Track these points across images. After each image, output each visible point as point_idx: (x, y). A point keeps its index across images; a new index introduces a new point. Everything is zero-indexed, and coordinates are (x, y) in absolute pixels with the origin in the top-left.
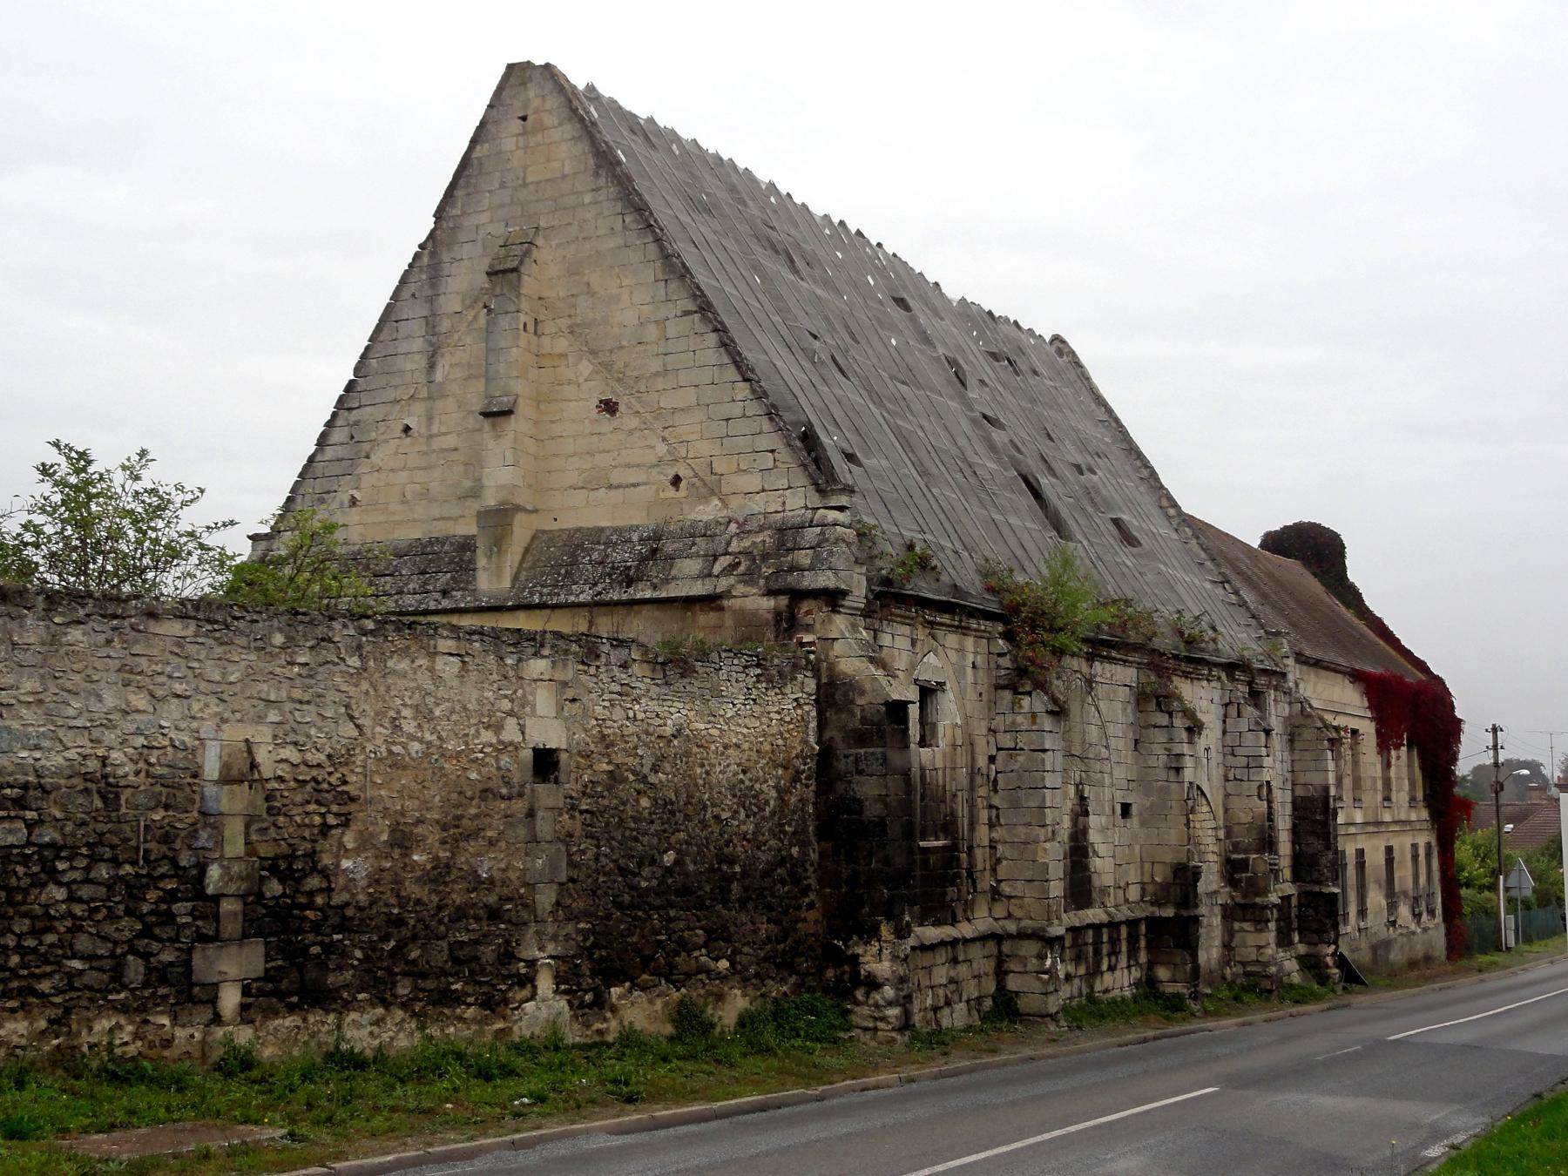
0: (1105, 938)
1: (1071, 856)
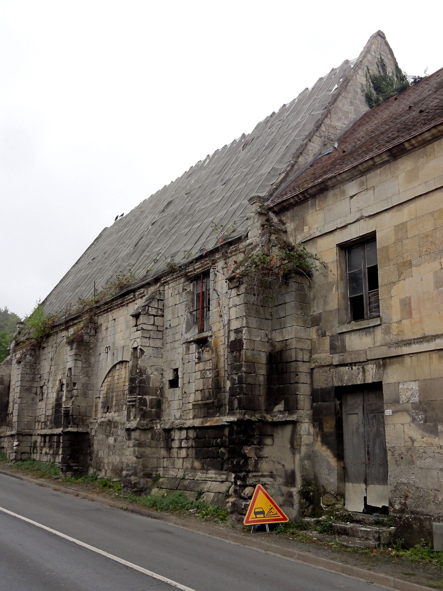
0: (47, 440)
1: (55, 407)
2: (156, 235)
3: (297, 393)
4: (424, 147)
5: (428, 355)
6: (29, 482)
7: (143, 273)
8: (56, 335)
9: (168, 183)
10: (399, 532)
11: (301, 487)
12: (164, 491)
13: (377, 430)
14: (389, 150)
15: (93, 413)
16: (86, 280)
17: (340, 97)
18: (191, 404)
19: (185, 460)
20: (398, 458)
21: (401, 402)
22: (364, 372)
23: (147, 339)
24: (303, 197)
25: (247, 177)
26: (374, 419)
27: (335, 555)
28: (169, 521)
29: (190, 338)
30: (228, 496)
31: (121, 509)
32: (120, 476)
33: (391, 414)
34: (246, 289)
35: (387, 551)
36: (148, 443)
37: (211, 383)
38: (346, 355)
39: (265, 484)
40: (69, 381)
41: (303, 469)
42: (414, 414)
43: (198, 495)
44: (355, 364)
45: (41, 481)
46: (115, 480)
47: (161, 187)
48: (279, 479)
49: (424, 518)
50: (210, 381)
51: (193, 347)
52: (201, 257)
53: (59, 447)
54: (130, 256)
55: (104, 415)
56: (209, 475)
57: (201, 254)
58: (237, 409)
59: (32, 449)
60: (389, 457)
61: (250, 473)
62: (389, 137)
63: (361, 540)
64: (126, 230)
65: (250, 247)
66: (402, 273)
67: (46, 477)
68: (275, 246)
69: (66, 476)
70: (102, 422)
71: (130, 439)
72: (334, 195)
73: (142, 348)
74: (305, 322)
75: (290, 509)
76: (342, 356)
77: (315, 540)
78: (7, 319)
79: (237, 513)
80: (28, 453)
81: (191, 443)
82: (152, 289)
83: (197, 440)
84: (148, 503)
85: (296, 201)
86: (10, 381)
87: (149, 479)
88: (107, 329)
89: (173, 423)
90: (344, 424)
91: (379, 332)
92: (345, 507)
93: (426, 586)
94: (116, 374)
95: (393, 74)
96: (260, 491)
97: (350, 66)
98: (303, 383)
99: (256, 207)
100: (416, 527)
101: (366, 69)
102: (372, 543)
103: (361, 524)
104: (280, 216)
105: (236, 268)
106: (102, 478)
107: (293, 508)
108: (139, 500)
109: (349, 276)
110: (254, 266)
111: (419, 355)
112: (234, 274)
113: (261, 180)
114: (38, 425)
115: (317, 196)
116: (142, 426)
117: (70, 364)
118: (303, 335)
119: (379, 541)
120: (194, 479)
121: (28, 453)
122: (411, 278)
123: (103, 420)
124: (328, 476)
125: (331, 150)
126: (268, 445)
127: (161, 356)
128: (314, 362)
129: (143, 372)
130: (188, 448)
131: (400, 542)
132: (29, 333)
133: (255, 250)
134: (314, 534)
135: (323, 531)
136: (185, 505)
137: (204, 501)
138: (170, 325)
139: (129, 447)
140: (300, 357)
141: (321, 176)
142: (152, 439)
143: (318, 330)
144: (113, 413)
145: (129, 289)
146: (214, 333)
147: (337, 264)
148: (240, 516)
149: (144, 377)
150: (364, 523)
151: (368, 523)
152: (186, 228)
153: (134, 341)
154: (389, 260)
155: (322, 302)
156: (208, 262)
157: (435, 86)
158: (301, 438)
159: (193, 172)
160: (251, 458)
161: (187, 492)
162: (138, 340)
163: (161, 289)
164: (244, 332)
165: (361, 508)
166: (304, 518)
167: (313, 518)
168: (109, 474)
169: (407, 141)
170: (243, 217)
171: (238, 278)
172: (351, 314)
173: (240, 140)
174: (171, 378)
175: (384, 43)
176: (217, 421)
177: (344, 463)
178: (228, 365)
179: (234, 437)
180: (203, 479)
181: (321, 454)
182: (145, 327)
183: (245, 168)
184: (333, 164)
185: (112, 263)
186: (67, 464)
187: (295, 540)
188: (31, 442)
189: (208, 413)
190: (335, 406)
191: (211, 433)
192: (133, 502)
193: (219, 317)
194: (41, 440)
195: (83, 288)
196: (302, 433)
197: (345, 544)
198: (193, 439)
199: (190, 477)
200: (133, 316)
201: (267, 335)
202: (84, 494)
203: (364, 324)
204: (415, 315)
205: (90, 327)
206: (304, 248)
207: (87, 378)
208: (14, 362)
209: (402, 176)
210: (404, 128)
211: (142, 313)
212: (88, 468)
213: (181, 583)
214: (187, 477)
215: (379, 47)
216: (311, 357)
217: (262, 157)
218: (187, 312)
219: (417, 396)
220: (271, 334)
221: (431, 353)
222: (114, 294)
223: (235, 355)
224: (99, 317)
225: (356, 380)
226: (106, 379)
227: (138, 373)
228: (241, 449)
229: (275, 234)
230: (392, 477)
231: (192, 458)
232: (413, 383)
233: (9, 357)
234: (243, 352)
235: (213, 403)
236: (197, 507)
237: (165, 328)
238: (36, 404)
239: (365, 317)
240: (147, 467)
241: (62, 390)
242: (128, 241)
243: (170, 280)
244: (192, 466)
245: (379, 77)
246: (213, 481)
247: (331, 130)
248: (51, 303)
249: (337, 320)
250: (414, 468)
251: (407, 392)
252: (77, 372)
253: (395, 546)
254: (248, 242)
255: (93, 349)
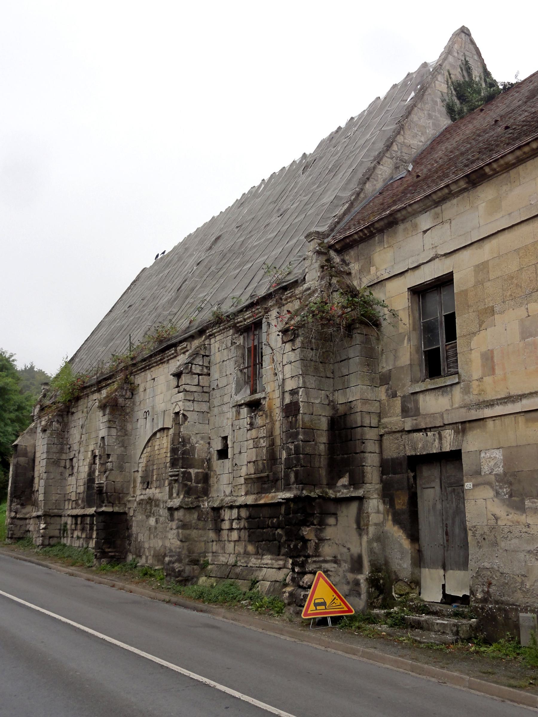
0: (79, 522)
1: (88, 483)
2: (202, 277)
3: (364, 464)
4: (508, 171)
5: (513, 418)
6: (58, 571)
7: (186, 324)
8: (86, 398)
9: (217, 214)
10: (482, 625)
11: (369, 573)
12: (213, 580)
13: (457, 506)
14: (467, 176)
15: (131, 490)
16: (121, 332)
17: (416, 109)
18: (243, 478)
19: (237, 543)
20: (480, 539)
21: (483, 474)
22: (440, 438)
23: (191, 403)
24: (369, 232)
25: (306, 207)
26: (453, 494)
27: (405, 652)
28: (218, 614)
29: (241, 400)
30: (286, 585)
31: (163, 601)
32: (163, 563)
33: (472, 487)
34: (302, 343)
35: (466, 647)
36: (193, 524)
37: (265, 453)
38: (420, 419)
39: (328, 571)
40: (102, 452)
41: (371, 553)
42: (498, 487)
43: (252, 584)
44: (430, 429)
45: (71, 569)
46: (157, 568)
47: (208, 219)
48: (345, 564)
49: (509, 608)
50: (264, 450)
51: (244, 411)
52: (251, 305)
53: (93, 530)
54: (171, 302)
55: (144, 492)
56: (265, 561)
57: (252, 301)
58: (293, 484)
59: (62, 532)
60: (470, 538)
61: (309, 558)
62: (468, 159)
63: (436, 634)
64: (167, 271)
65: (308, 292)
66: (483, 322)
67: (77, 564)
68: (337, 291)
69: (100, 564)
70: (142, 500)
71: (172, 520)
72: (405, 229)
73: (185, 413)
74: (372, 380)
75: (357, 599)
76: (415, 420)
77: (384, 635)
78: (33, 377)
79: (295, 605)
80: (57, 537)
81: (243, 523)
82: (196, 343)
83: (250, 520)
84: (194, 594)
85: (360, 237)
86: (35, 452)
87: (195, 567)
88: (145, 390)
89: (222, 500)
90: (419, 500)
91: (457, 390)
92: (421, 596)
93: (505, 685)
94: (157, 443)
95: (481, 78)
96: (321, 579)
97: (429, 70)
98: (370, 452)
99: (313, 245)
100: (501, 618)
101: (447, 74)
102: (449, 637)
103: (438, 616)
104: (342, 255)
105: (291, 319)
106: (142, 566)
107: (360, 599)
108: (183, 591)
109: (423, 326)
110: (311, 315)
111: (503, 418)
112: (287, 326)
113: (323, 210)
114: (69, 504)
115: (385, 231)
116: (186, 505)
117: (103, 433)
118: (370, 395)
119: (458, 635)
120: (247, 566)
121: (57, 537)
122: (493, 328)
123: (142, 497)
124: (401, 560)
125: (404, 174)
126: (330, 525)
127: (207, 422)
128: (384, 428)
129: (186, 441)
130: (239, 529)
131: (481, 636)
132: (56, 395)
133: (313, 296)
134: (383, 628)
135: (394, 624)
136: (237, 596)
137: (258, 591)
138: (217, 385)
139: (171, 529)
140: (367, 422)
141: (389, 207)
142: (199, 519)
143: (387, 390)
144: (153, 489)
145: (169, 343)
146: (268, 395)
147: (409, 312)
148: (298, 608)
149: (188, 446)
150: (442, 615)
151: (446, 614)
152: (235, 269)
153: (176, 405)
154: (468, 306)
155: (392, 357)
156: (260, 310)
157: (526, 95)
158: (368, 517)
159: (245, 200)
160: (310, 540)
161: (240, 581)
162: (180, 404)
163: (206, 343)
164: (300, 394)
165: (439, 598)
166: (373, 610)
167: (384, 609)
168: (150, 561)
169: (487, 165)
170: (300, 256)
171: (293, 329)
172: (426, 370)
173: (301, 161)
174: (219, 448)
175: (469, 41)
176: (273, 498)
177: (419, 545)
178: (283, 432)
179: (291, 516)
180: (258, 566)
181: (393, 535)
182: (188, 388)
183: (304, 196)
184: (404, 192)
185: (151, 312)
186: (102, 549)
187: (361, 635)
188: (61, 524)
189: (262, 488)
190: (408, 479)
191: (266, 512)
192: (177, 593)
193: (273, 375)
194: (72, 521)
195: (118, 342)
196: (370, 510)
197: (419, 639)
198: (246, 519)
199: (242, 563)
200: (174, 375)
201: (327, 396)
202: (120, 584)
203: (440, 382)
204: (498, 371)
205: (125, 388)
206: (371, 293)
207: (123, 448)
208: (39, 430)
209: (482, 206)
210: (486, 148)
211: (184, 372)
212: (126, 554)
213: (221, 683)
214: (239, 564)
215: (463, 46)
216: (379, 421)
217: (325, 183)
218: (237, 370)
219: (501, 467)
220: (333, 395)
221: (516, 415)
222: (152, 348)
223: (290, 420)
224: (136, 377)
225: (432, 448)
226: (145, 450)
227: (180, 442)
228: (299, 530)
229: (337, 277)
230: (473, 561)
231: (245, 541)
232: (497, 451)
233: (33, 425)
234: (300, 417)
235: (268, 476)
236: (251, 598)
237: (211, 389)
238: (65, 479)
239: (442, 374)
240: (193, 553)
241: (94, 463)
242: (169, 285)
243: (216, 332)
244: (245, 551)
245: (463, 83)
246: (269, 568)
247: (405, 150)
248: (81, 360)
249: (409, 378)
250: (498, 550)
251: (490, 462)
252: (111, 442)
253: (475, 641)
254: (305, 286)
255: (129, 414)
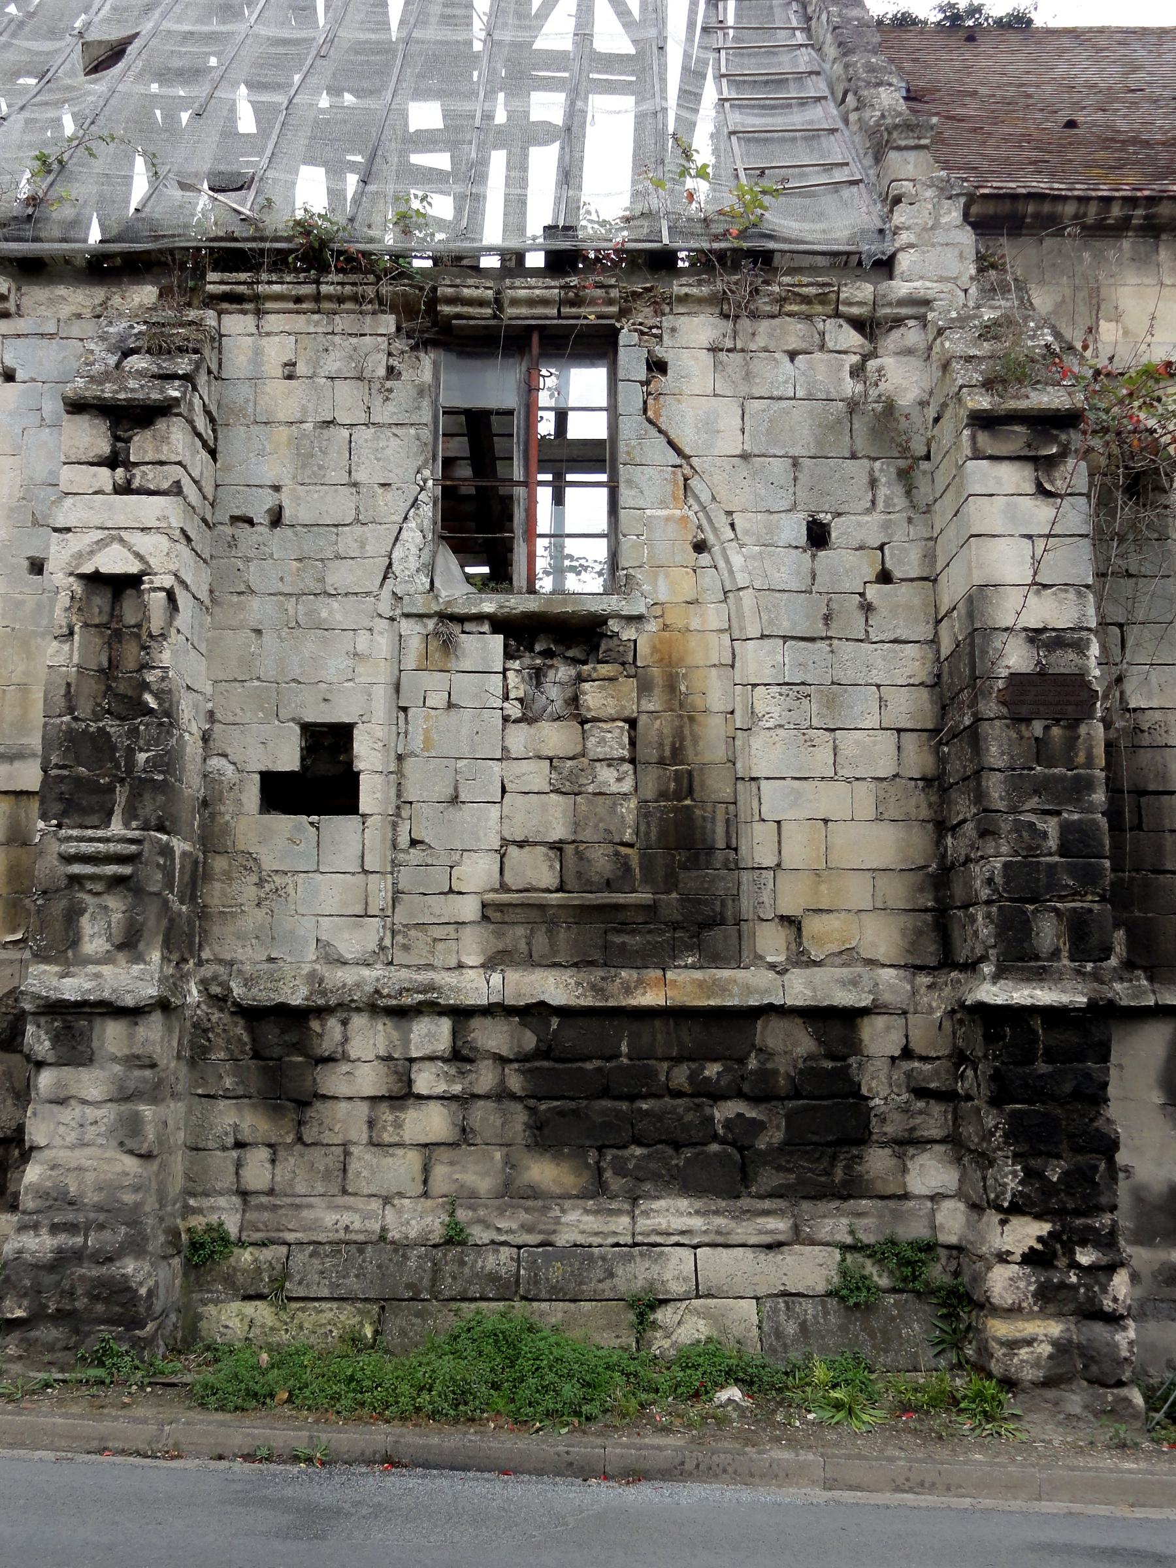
115: (1164, 237)
